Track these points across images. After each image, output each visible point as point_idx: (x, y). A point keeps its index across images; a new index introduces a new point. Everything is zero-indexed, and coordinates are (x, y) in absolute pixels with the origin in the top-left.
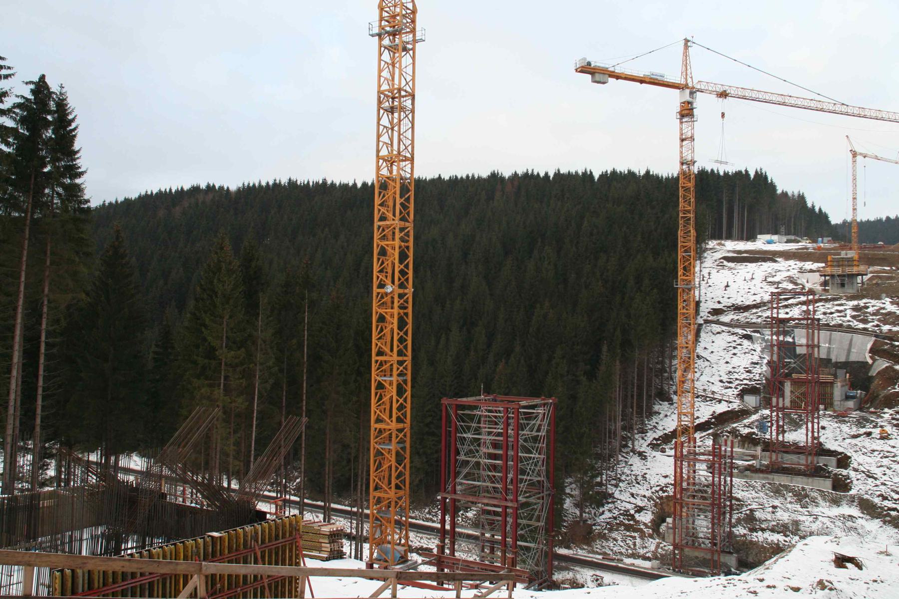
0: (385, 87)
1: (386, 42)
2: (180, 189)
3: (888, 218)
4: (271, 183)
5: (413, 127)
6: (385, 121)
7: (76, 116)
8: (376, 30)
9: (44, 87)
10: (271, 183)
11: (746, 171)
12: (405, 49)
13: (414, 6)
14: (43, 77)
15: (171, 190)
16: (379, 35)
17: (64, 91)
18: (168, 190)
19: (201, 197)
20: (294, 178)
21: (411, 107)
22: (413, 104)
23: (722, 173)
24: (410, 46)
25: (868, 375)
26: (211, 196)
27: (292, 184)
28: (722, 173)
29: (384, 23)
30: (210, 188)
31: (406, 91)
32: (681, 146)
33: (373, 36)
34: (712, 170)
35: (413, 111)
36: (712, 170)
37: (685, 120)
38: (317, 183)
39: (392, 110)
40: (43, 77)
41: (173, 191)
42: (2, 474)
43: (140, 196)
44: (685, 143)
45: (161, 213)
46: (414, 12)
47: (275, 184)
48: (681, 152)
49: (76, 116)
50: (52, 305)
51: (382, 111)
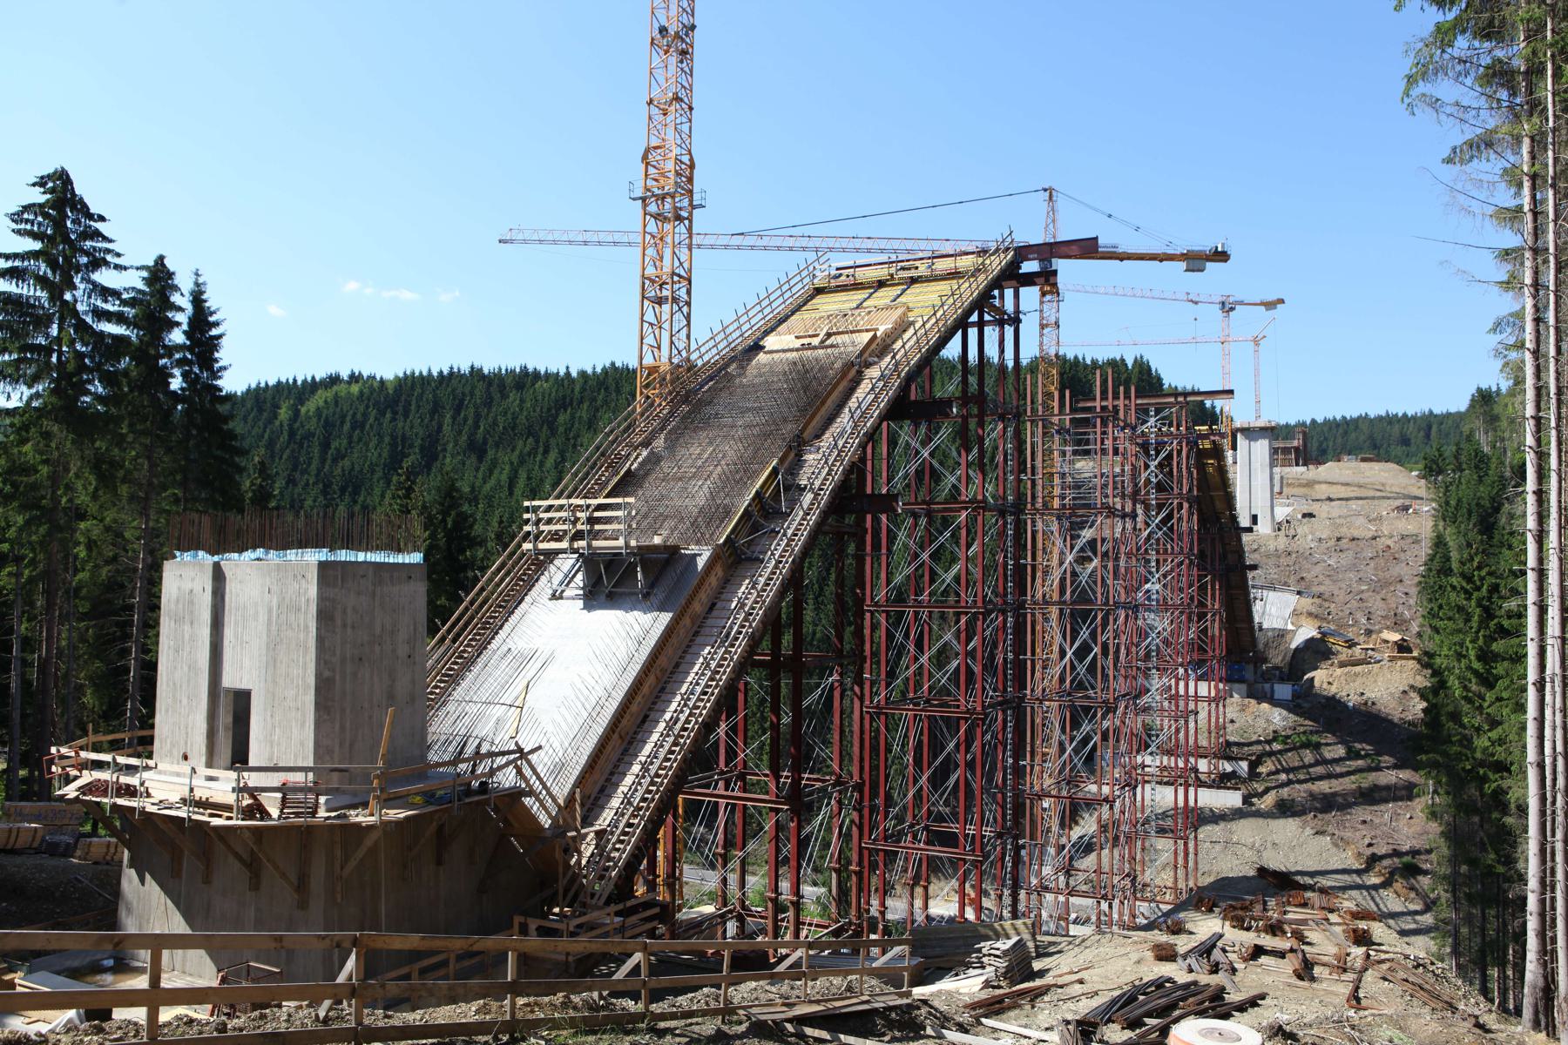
0: (650, 271)
1: (653, 208)
2: (309, 379)
3: (1313, 421)
4: (446, 372)
5: (689, 325)
6: (650, 317)
7: (198, 299)
8: (639, 193)
9: (162, 272)
10: (446, 372)
11: (1123, 360)
12: (679, 218)
13: (691, 160)
14: (161, 258)
15: (295, 380)
16: (644, 199)
17: (201, 280)
18: (291, 381)
19: (341, 389)
20: (477, 365)
21: (686, 297)
22: (689, 292)
23: (1088, 362)
24: (684, 214)
25: (1288, 648)
26: (355, 389)
27: (476, 373)
28: (1088, 362)
29: (650, 183)
30: (355, 378)
31: (679, 276)
32: (1042, 335)
33: (634, 199)
34: (1076, 357)
35: (688, 304)
36: (1076, 357)
37: (1048, 297)
38: (513, 371)
39: (660, 301)
40: (161, 258)
41: (299, 383)
42: (4, 771)
43: (249, 390)
44: (1045, 331)
45: (284, 413)
46: (692, 166)
47: (451, 373)
48: (1041, 344)
49: (198, 299)
50: (880, 858)
51: (646, 303)
